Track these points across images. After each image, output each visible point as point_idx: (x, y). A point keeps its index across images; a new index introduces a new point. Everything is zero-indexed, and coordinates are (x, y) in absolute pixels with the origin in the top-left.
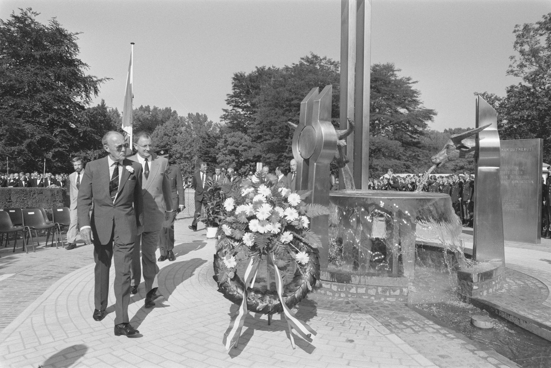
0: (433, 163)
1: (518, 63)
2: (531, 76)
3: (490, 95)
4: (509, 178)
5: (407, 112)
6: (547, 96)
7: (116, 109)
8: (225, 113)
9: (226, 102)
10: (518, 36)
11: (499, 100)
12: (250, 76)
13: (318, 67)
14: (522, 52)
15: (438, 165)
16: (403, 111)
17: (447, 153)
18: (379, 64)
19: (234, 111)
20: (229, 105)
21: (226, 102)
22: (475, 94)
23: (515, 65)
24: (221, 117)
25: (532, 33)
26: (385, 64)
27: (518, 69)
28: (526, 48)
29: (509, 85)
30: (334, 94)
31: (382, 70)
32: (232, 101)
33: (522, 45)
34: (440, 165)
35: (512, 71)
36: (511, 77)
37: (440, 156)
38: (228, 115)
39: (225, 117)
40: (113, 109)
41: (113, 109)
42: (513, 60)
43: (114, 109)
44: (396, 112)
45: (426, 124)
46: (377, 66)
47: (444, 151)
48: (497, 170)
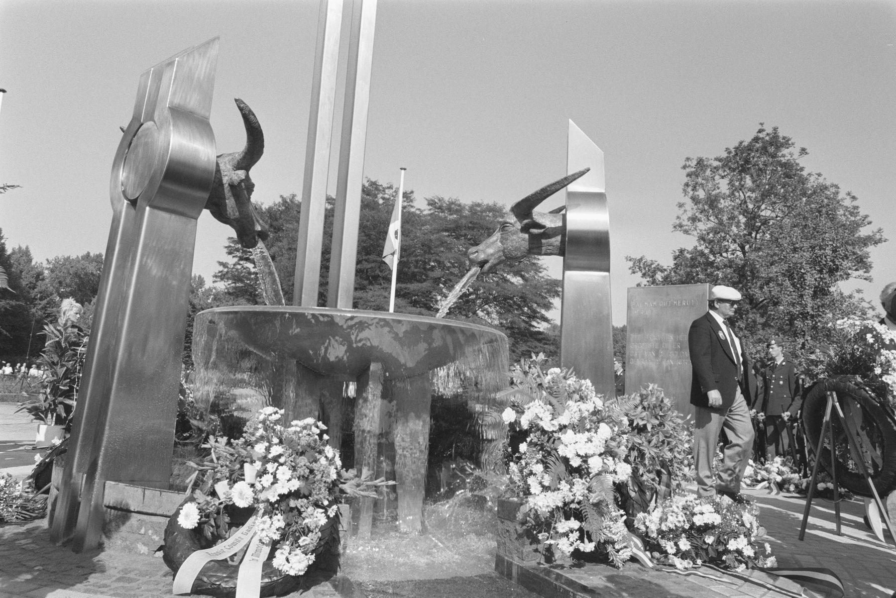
0: (473, 263)
1: (690, 214)
2: (708, 234)
3: (649, 263)
4: (657, 356)
5: (521, 282)
6: (730, 267)
7: (27, 248)
8: (221, 268)
9: (226, 250)
10: (689, 175)
11: (662, 271)
12: (270, 210)
13: (381, 201)
14: (695, 200)
15: (482, 264)
16: (517, 280)
17: (503, 240)
18: (480, 202)
19: (239, 267)
20: (231, 256)
21: (226, 250)
22: (626, 258)
23: (685, 217)
24: (216, 276)
25: (708, 172)
26: (491, 203)
27: (689, 223)
28: (701, 194)
29: (677, 248)
30: (404, 243)
31: (484, 211)
32: (237, 250)
33: (694, 189)
34: (487, 267)
35: (681, 226)
36: (679, 234)
37: (488, 247)
38: (227, 272)
39: (222, 276)
40: (20, 248)
41: (20, 248)
42: (683, 209)
43: (24, 247)
44: (506, 281)
45: (551, 303)
46: (479, 205)
47: (497, 236)
48: (605, 277)
